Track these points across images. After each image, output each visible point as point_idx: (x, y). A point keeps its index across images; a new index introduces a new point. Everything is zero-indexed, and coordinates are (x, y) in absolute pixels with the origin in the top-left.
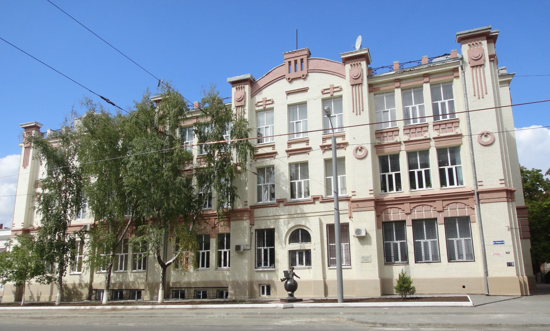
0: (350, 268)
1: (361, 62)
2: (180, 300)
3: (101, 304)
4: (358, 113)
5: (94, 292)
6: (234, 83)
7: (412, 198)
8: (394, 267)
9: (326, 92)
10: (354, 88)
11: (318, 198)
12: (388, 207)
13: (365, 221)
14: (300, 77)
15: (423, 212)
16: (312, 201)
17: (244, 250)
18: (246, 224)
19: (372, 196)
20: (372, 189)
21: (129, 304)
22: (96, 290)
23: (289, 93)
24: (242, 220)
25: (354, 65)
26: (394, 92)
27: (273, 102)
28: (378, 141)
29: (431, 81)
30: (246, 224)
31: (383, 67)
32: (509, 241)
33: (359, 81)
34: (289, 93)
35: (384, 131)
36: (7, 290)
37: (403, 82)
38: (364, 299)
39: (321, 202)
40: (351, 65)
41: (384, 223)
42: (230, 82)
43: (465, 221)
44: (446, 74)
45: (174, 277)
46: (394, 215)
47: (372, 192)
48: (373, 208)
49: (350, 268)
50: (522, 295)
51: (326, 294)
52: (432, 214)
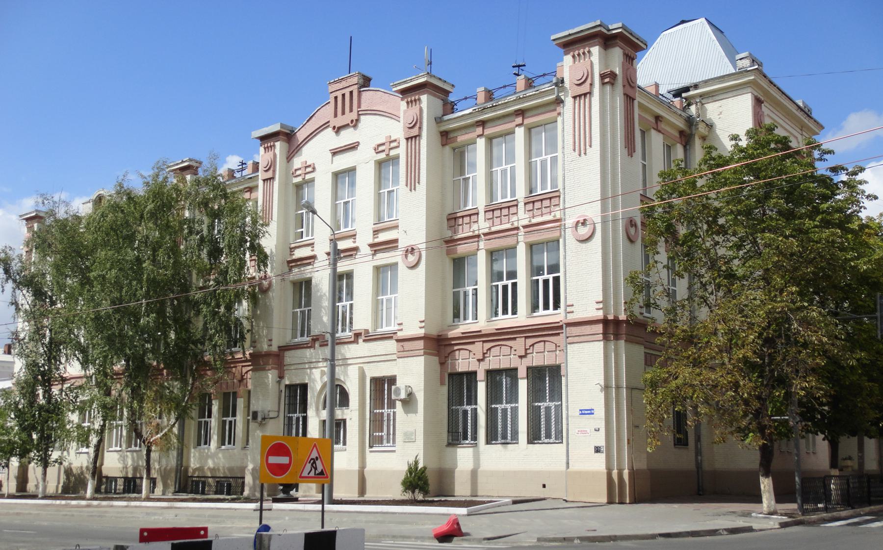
0: (394, 451)
1: (592, 49)
2: (198, 497)
3: (84, 498)
4: (582, 152)
5: (104, 480)
6: (264, 139)
7: (483, 333)
8: (458, 450)
9: (381, 148)
10: (577, 102)
11: (360, 334)
12: (456, 348)
13: (412, 373)
14: (348, 125)
15: (500, 359)
16: (352, 339)
17: (264, 419)
18: (271, 376)
19: (422, 332)
20: (423, 319)
21: (130, 499)
22: (107, 477)
23: (335, 153)
24: (264, 369)
25: (411, 101)
27: (314, 168)
28: (448, 234)
29: (526, 121)
30: (271, 376)
31: (466, 98)
32: (600, 412)
33: (585, 88)
34: (335, 153)
35: (459, 215)
36: (7, 475)
37: (488, 125)
38: (374, 501)
39: (364, 341)
40: (574, 57)
41: (451, 375)
42: (257, 138)
43: (555, 372)
44: (543, 110)
45: (194, 460)
46: (464, 362)
47: (423, 324)
48: (601, 337)
50: (610, 502)
51: (362, 490)
52: (514, 362)
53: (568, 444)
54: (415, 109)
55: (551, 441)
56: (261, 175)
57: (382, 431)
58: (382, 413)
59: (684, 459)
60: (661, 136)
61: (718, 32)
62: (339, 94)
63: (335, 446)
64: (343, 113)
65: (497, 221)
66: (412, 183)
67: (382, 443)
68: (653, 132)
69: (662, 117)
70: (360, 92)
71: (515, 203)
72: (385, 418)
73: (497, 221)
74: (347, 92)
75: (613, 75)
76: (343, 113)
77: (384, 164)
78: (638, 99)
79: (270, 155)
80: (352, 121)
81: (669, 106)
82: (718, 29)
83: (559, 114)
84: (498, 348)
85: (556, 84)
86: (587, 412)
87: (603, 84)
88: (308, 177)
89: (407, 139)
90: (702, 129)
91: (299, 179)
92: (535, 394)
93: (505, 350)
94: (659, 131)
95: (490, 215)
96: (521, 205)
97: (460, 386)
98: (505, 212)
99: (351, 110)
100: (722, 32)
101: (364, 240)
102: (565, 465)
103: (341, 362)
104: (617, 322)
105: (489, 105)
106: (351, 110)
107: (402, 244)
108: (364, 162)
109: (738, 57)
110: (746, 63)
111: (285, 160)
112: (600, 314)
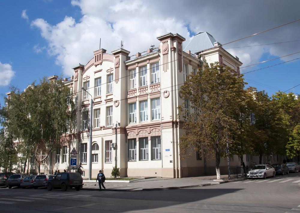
9: (108, 71)
13: (117, 139)
15: (143, 134)
16: (100, 129)
25: (117, 57)
26: (136, 69)
27: (89, 77)
31: (133, 56)
33: (166, 52)
43: (159, 137)
49: (86, 164)
50: (175, 177)
53: (162, 160)
54: (118, 59)
55: (158, 159)
56: (74, 80)
57: (109, 157)
58: (109, 152)
59: (201, 164)
60: (191, 66)
61: (211, 37)
62: (97, 55)
63: (92, 163)
64: (98, 61)
65: (142, 92)
66: (117, 80)
67: (109, 161)
68: (189, 65)
69: (192, 61)
70: (102, 54)
71: (147, 87)
72: (110, 153)
73: (142, 92)
74: (99, 54)
75: (174, 48)
76: (98, 61)
77: (109, 76)
78: (183, 55)
79: (77, 73)
80: (100, 63)
81: (194, 58)
82: (208, 34)
83: (159, 60)
84: (155, 129)
85: (158, 51)
86: (168, 150)
87: (171, 51)
88: (88, 80)
89: (115, 68)
90: (204, 64)
91: (85, 81)
92: (154, 145)
93: (144, 131)
94: (191, 65)
95: (140, 90)
96: (137, 90)
97: (128, 143)
98: (133, 92)
99: (100, 60)
100: (212, 36)
101: (104, 98)
102: (162, 166)
103: (94, 137)
104: (177, 123)
105: (139, 57)
106: (100, 60)
107: (114, 100)
108: (103, 76)
109: (214, 43)
110: (216, 45)
111: (126, 70)
112: (171, 120)
